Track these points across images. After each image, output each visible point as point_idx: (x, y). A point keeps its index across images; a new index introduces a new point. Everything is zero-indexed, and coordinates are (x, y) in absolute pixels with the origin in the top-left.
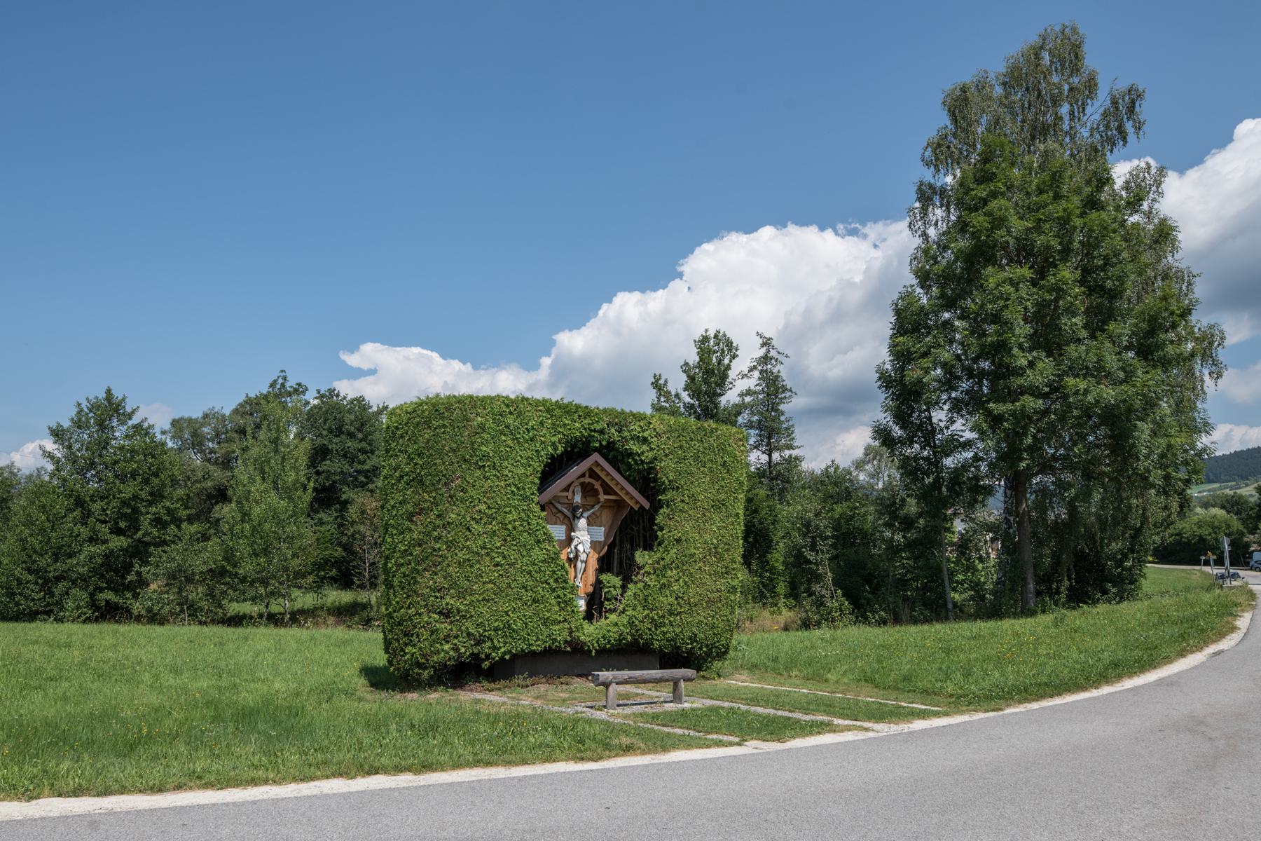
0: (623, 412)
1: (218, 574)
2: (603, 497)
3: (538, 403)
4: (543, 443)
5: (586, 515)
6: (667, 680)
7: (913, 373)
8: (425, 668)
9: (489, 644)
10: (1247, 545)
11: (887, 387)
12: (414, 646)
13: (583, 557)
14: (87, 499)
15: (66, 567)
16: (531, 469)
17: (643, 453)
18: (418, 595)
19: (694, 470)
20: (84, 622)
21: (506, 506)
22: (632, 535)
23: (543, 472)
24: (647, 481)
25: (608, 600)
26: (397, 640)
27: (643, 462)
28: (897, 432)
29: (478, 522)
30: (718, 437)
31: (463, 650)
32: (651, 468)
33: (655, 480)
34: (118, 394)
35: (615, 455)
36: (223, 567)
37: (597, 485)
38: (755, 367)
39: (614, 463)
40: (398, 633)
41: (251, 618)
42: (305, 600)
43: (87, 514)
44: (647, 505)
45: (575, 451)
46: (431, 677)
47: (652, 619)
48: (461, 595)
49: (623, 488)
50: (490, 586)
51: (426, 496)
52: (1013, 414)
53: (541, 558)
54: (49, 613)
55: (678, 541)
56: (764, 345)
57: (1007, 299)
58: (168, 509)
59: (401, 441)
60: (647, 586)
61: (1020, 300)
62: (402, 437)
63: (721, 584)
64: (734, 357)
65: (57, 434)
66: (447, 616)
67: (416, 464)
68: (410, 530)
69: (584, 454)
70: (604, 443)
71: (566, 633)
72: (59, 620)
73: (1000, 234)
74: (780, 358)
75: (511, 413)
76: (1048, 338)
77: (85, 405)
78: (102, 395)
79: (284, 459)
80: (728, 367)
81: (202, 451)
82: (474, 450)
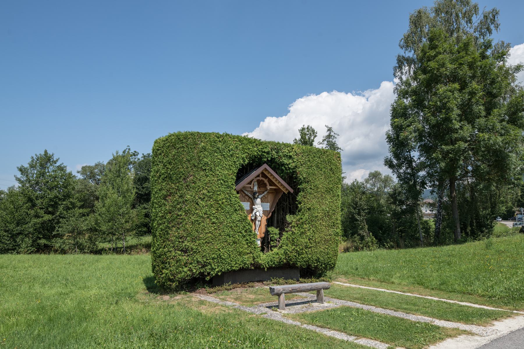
0: (279, 143)
1: (93, 230)
2: (269, 187)
3: (234, 137)
4: (237, 157)
5: (260, 196)
6: (314, 290)
7: (402, 135)
8: (173, 282)
9: (209, 267)
10: (514, 212)
11: (390, 142)
12: (167, 269)
13: (259, 218)
14: (34, 198)
15: (22, 229)
16: (231, 171)
17: (289, 164)
18: (169, 241)
19: (316, 172)
20: (30, 253)
21: (217, 191)
22: (285, 206)
23: (238, 173)
24: (292, 179)
25: (273, 241)
26: (158, 266)
27: (289, 168)
28: (395, 162)
29: (202, 200)
30: (328, 156)
31: (195, 271)
32: (294, 172)
33: (296, 178)
34: (50, 152)
35: (272, 162)
36: (95, 228)
37: (266, 181)
38: (325, 140)
39: (274, 169)
40: (160, 261)
41: (106, 250)
42: (131, 240)
43: (34, 205)
44: (292, 191)
45: (254, 163)
46: (177, 286)
47: (297, 250)
48: (193, 240)
49: (279, 182)
50: (210, 235)
51: (173, 186)
52: (453, 150)
53: (237, 219)
54: (14, 250)
55: (309, 209)
56: (328, 130)
57: (449, 98)
58: (71, 202)
59: (160, 157)
60: (293, 233)
61: (455, 98)
62: (160, 154)
63: (331, 231)
64: (315, 136)
65: (22, 170)
66: (185, 252)
67: (168, 168)
68: (165, 205)
69: (259, 165)
70: (269, 159)
71: (251, 259)
72: (18, 253)
74: (336, 136)
75: (220, 141)
76: (467, 115)
77: (35, 157)
78: (43, 153)
79: (122, 179)
80: (313, 141)
81: (95, 180)
82: (200, 160)
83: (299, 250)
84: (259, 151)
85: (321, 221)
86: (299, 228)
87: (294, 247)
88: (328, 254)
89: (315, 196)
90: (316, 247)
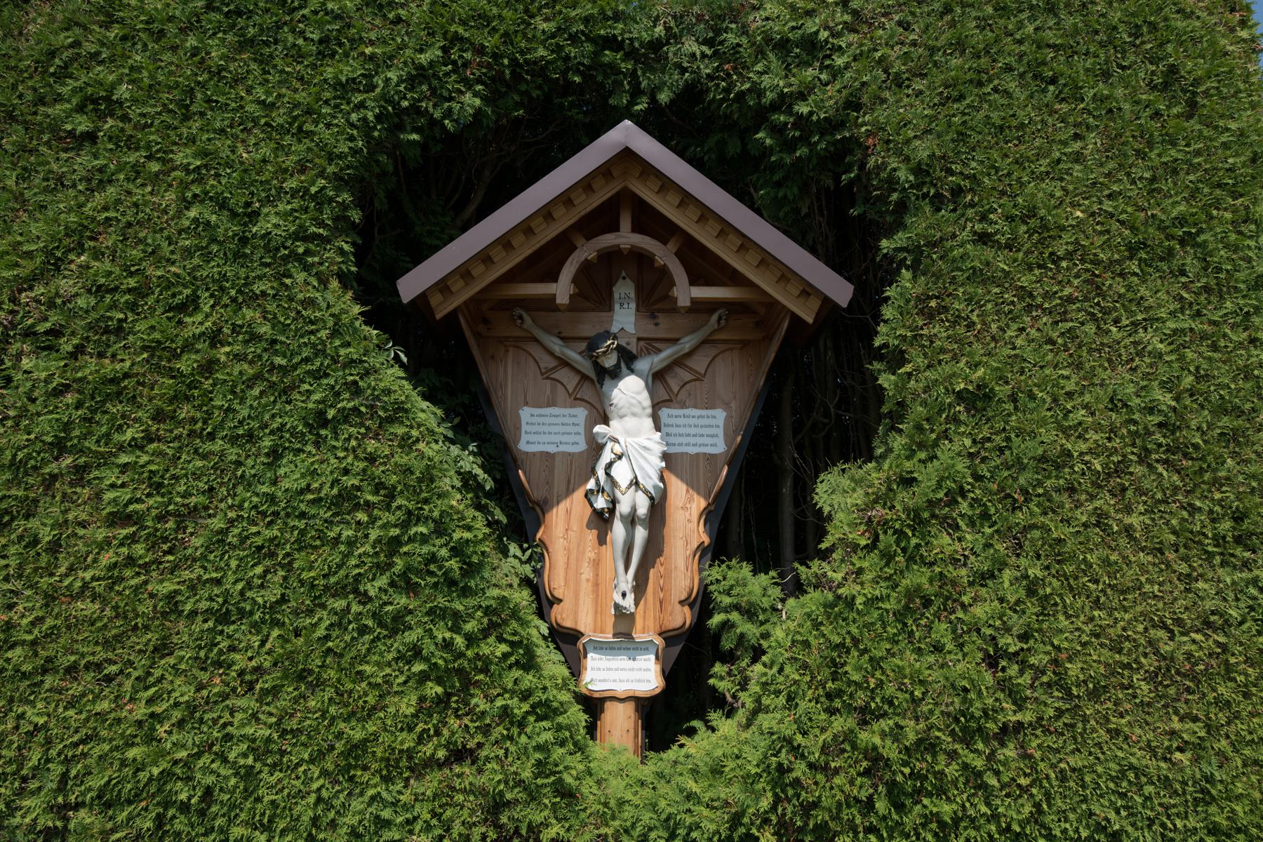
2: (686, 293)
24: (839, 203)
37: (664, 255)
44: (841, 291)
47: (876, 761)
50: (86, 607)
55: (978, 399)
73: (942, 758)
83: (891, 751)
84: (573, 38)
85: (1104, 501)
86: (888, 557)
87: (840, 724)
88: (1206, 798)
89: (1024, 293)
90: (1070, 722)
